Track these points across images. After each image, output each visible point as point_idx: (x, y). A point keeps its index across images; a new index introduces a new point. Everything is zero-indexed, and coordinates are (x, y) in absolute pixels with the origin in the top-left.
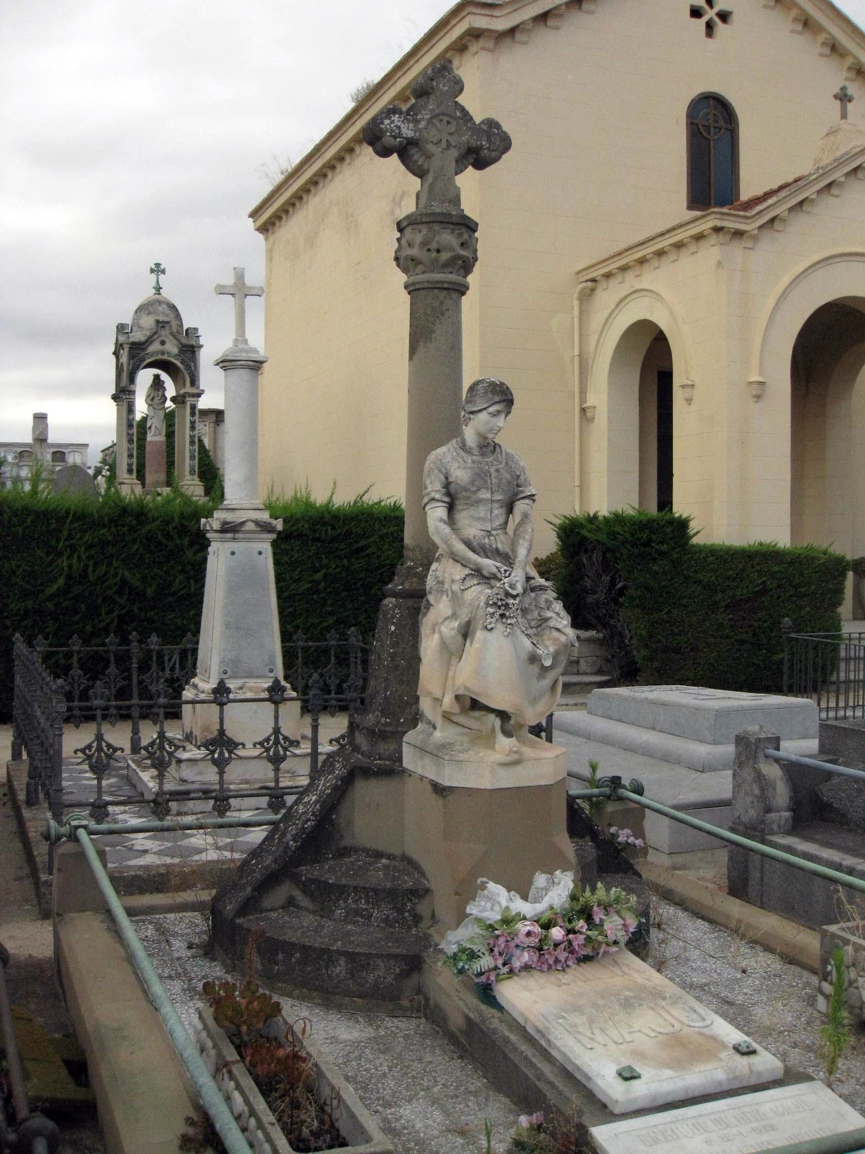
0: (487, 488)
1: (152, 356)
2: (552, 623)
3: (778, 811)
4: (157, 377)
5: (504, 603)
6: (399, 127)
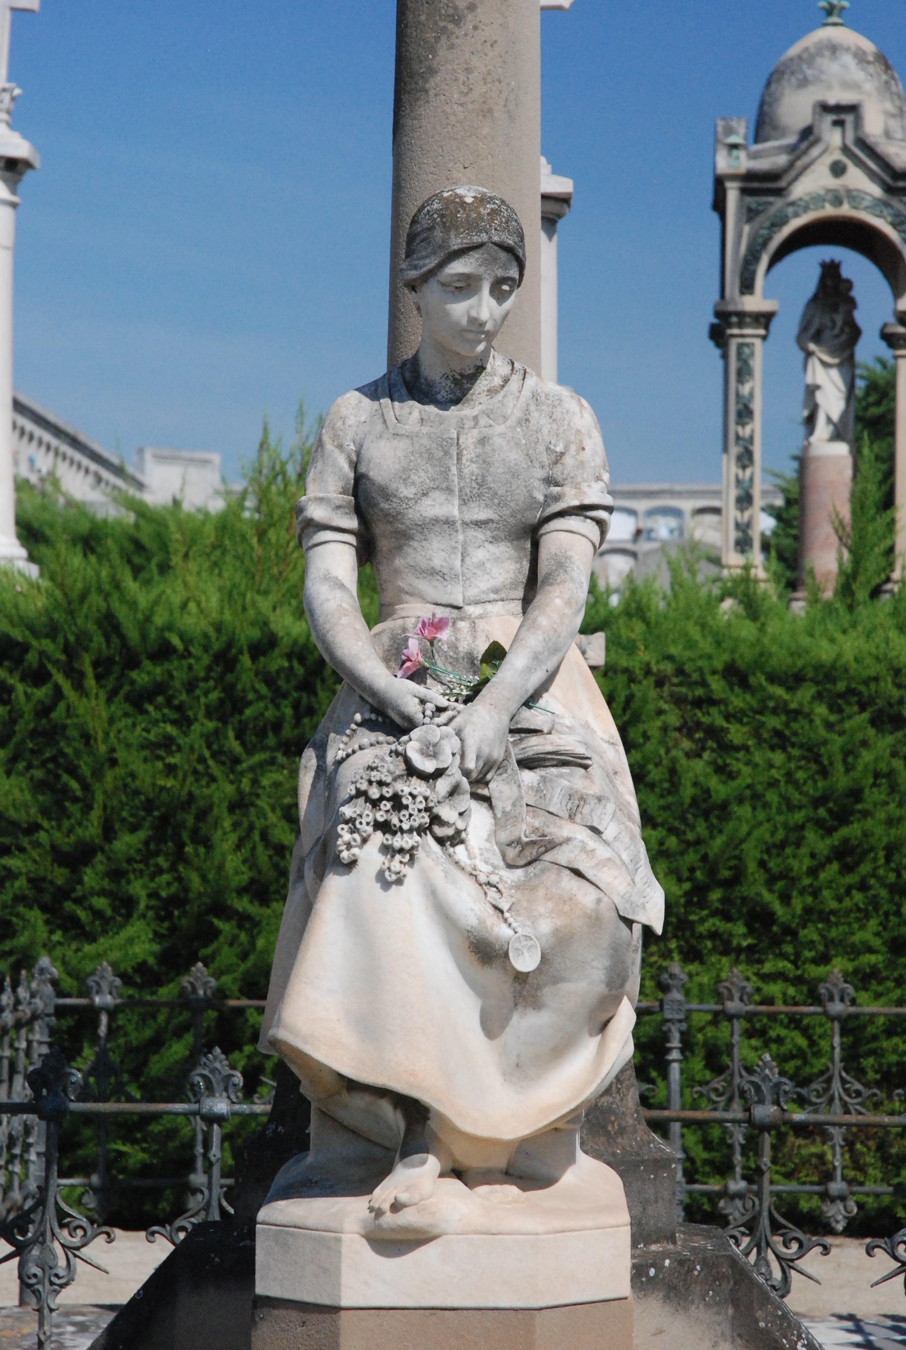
0: (449, 490)
1: (806, 209)
2: (562, 855)
4: (831, 270)
5: (388, 792)
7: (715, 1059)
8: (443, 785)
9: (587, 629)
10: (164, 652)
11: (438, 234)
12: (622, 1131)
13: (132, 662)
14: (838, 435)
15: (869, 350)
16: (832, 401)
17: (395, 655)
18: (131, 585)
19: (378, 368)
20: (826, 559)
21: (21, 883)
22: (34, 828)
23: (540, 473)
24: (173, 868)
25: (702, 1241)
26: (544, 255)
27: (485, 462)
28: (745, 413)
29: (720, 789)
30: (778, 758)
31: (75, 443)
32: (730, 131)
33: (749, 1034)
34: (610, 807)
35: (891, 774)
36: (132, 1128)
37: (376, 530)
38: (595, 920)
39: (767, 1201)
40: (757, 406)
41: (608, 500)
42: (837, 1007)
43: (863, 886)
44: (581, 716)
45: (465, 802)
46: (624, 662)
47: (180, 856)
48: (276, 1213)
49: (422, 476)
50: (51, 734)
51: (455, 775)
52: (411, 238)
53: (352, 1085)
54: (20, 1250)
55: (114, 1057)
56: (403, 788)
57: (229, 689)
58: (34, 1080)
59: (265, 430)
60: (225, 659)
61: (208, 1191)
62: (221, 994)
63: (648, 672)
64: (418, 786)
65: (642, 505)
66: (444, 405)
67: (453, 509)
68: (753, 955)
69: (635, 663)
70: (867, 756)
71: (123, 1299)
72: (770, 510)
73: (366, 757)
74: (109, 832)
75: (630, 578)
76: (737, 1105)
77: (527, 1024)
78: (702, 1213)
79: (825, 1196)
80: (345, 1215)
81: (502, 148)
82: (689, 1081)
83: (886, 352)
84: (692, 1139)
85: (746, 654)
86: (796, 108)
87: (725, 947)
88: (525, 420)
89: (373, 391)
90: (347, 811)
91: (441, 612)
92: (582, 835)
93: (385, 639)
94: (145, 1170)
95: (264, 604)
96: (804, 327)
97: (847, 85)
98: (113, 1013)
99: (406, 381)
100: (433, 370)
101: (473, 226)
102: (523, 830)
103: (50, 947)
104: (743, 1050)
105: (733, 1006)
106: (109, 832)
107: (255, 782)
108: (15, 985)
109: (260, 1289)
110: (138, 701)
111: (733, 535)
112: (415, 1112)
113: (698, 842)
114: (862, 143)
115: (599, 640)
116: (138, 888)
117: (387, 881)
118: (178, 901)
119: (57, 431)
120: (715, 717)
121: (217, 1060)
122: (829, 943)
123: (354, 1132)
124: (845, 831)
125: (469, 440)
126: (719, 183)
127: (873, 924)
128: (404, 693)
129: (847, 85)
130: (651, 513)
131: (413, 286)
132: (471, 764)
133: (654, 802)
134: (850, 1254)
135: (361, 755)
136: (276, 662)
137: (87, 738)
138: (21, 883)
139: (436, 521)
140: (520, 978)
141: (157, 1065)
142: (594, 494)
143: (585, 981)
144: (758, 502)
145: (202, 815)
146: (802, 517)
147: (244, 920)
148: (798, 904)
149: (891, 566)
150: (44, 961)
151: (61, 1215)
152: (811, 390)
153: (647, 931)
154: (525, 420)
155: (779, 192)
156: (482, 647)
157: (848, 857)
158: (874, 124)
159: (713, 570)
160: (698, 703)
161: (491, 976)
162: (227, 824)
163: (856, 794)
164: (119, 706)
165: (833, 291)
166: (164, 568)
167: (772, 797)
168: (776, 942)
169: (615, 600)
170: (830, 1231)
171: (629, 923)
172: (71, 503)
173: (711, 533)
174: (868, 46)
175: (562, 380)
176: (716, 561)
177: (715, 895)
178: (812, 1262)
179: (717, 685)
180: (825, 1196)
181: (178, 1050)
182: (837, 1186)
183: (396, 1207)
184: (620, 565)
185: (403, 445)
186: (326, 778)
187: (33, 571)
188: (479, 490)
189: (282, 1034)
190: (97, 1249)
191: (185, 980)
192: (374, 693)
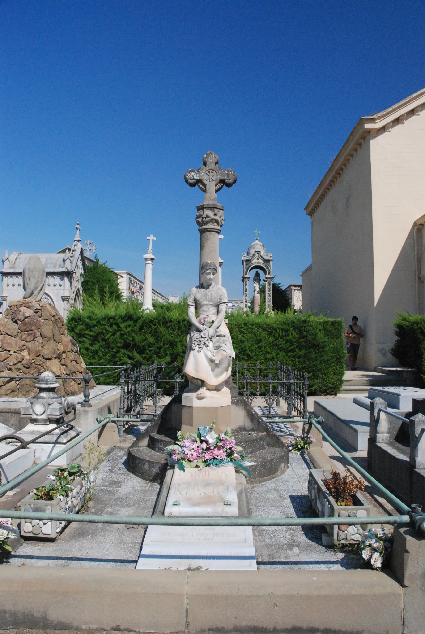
2: (222, 348)
3: (382, 433)
4: (257, 272)
6: (193, 176)
7: (243, 374)
8: (206, 339)
9: (225, 318)
10: (171, 321)
11: (205, 267)
12: (230, 384)
13: (167, 323)
14: (258, 293)
15: (262, 282)
16: (257, 289)
17: (200, 322)
18: (167, 313)
19: (198, 284)
20: (257, 309)
21: (153, 351)
22: (155, 344)
23: (219, 298)
24: (172, 349)
25: (240, 398)
26: (219, 270)
27: (212, 297)
28: (246, 290)
29: (243, 339)
30: (251, 335)
31: (160, 294)
32: (244, 254)
33: (247, 371)
34: (228, 342)
35: (265, 337)
36: (167, 383)
37: (197, 305)
38: (226, 357)
39: (249, 392)
40: (248, 289)
41: (228, 301)
42: (258, 367)
43: (261, 351)
44: (224, 330)
45: (209, 341)
46: (231, 322)
47: (173, 348)
48: (185, 395)
49: (203, 298)
50: (156, 332)
51: (208, 338)
52: (202, 268)
53: (194, 378)
54: (153, 398)
55: (165, 374)
56: (201, 339)
57: (179, 326)
58: (154, 377)
59: (106, 263)
60: (179, 322)
61: (177, 391)
62: (178, 366)
63: (234, 324)
64: (203, 339)
65: (233, 302)
66: (206, 289)
67: (207, 303)
68: (248, 360)
69: (232, 323)
70: (262, 335)
71: (166, 404)
72: (249, 303)
73: (196, 335)
74: (164, 345)
75: (232, 312)
76: (245, 380)
77: (217, 370)
78: (241, 394)
79: (257, 391)
80: (194, 395)
81: (213, 256)
82: (239, 377)
83: (264, 283)
84: (240, 384)
85: (246, 322)
86: (252, 251)
87: (244, 359)
88: (217, 291)
89: (197, 287)
90: (194, 342)
91: (206, 316)
92: (224, 345)
93: (199, 320)
94: (169, 388)
95: (184, 315)
96: (254, 279)
97: (259, 249)
98: (165, 368)
99: (201, 286)
100: (205, 284)
101: (210, 266)
102: (217, 345)
103: (157, 360)
104: (246, 373)
105: (245, 367)
106: (164, 345)
107: (183, 338)
108: (152, 365)
109: (183, 404)
110: (168, 328)
111: (245, 306)
112: (203, 382)
113: (240, 346)
114: (261, 256)
115: (227, 319)
116: (168, 352)
117: (199, 352)
118: (173, 354)
119: (158, 293)
120: (243, 330)
121: (178, 375)
122: (257, 359)
123: (195, 384)
124: (259, 344)
125: (209, 294)
126: (243, 261)
127: (263, 356)
128: (201, 327)
129: (259, 249)
130: (235, 303)
131: (202, 274)
132: (210, 336)
133: (234, 341)
134: (259, 398)
135: (195, 335)
136: (186, 323)
137: (161, 333)
138: (153, 351)
139: (205, 304)
140: (216, 364)
141: (170, 375)
142: (226, 301)
143: (225, 364)
144: (248, 302)
145: (176, 343)
146: (254, 304)
147: (182, 356)
148: (253, 354)
149: (265, 310)
150: (156, 362)
151: (158, 394)
152: (255, 287)
153: (233, 358)
154: (217, 291)
155: (250, 262)
156: (211, 321)
157: (260, 347)
158: (262, 254)
159: (242, 310)
160: (241, 328)
161: (213, 364)
162: (179, 344)
163: (261, 339)
164: (165, 329)
165: (257, 275)
166: (171, 311)
167: (250, 340)
168: (250, 359)
169: (230, 314)
170: (256, 395)
171: (231, 357)
172: (160, 302)
173: (242, 306)
174: (261, 244)
175: (222, 286)
176: (243, 309)
177: (243, 353)
178: (255, 400)
179: (243, 325)
180: (257, 391)
181: (173, 373)
182: (258, 390)
183: (200, 394)
184: (231, 310)
185: (201, 294)
186: (191, 338)
187: (154, 311)
188: (211, 300)
189: (185, 372)
190: (162, 398)
191: (174, 364)
192: (197, 327)
